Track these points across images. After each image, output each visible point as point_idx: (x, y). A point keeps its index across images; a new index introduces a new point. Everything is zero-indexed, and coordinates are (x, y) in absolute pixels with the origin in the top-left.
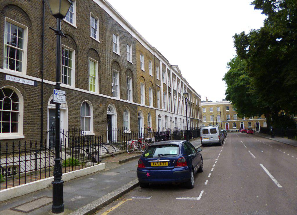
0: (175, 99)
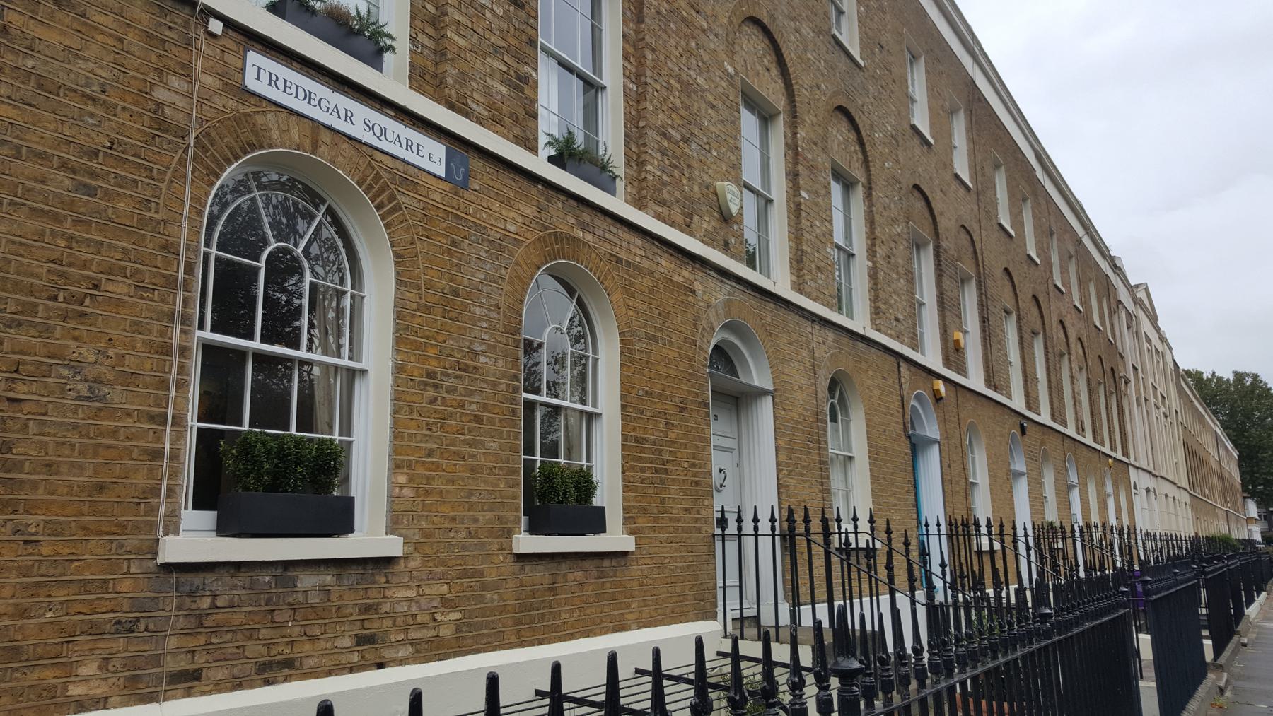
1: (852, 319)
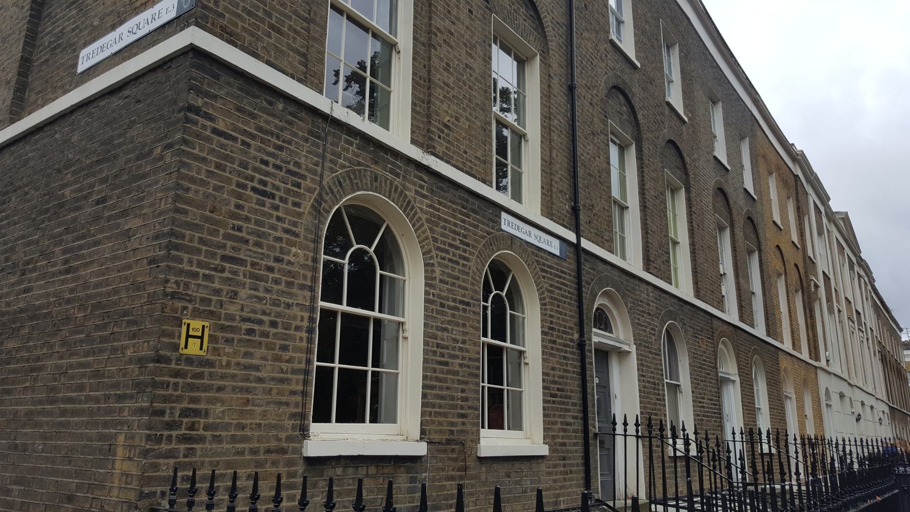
0: (853, 333)
1: (387, 128)
